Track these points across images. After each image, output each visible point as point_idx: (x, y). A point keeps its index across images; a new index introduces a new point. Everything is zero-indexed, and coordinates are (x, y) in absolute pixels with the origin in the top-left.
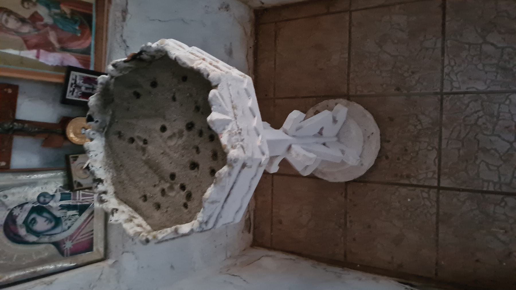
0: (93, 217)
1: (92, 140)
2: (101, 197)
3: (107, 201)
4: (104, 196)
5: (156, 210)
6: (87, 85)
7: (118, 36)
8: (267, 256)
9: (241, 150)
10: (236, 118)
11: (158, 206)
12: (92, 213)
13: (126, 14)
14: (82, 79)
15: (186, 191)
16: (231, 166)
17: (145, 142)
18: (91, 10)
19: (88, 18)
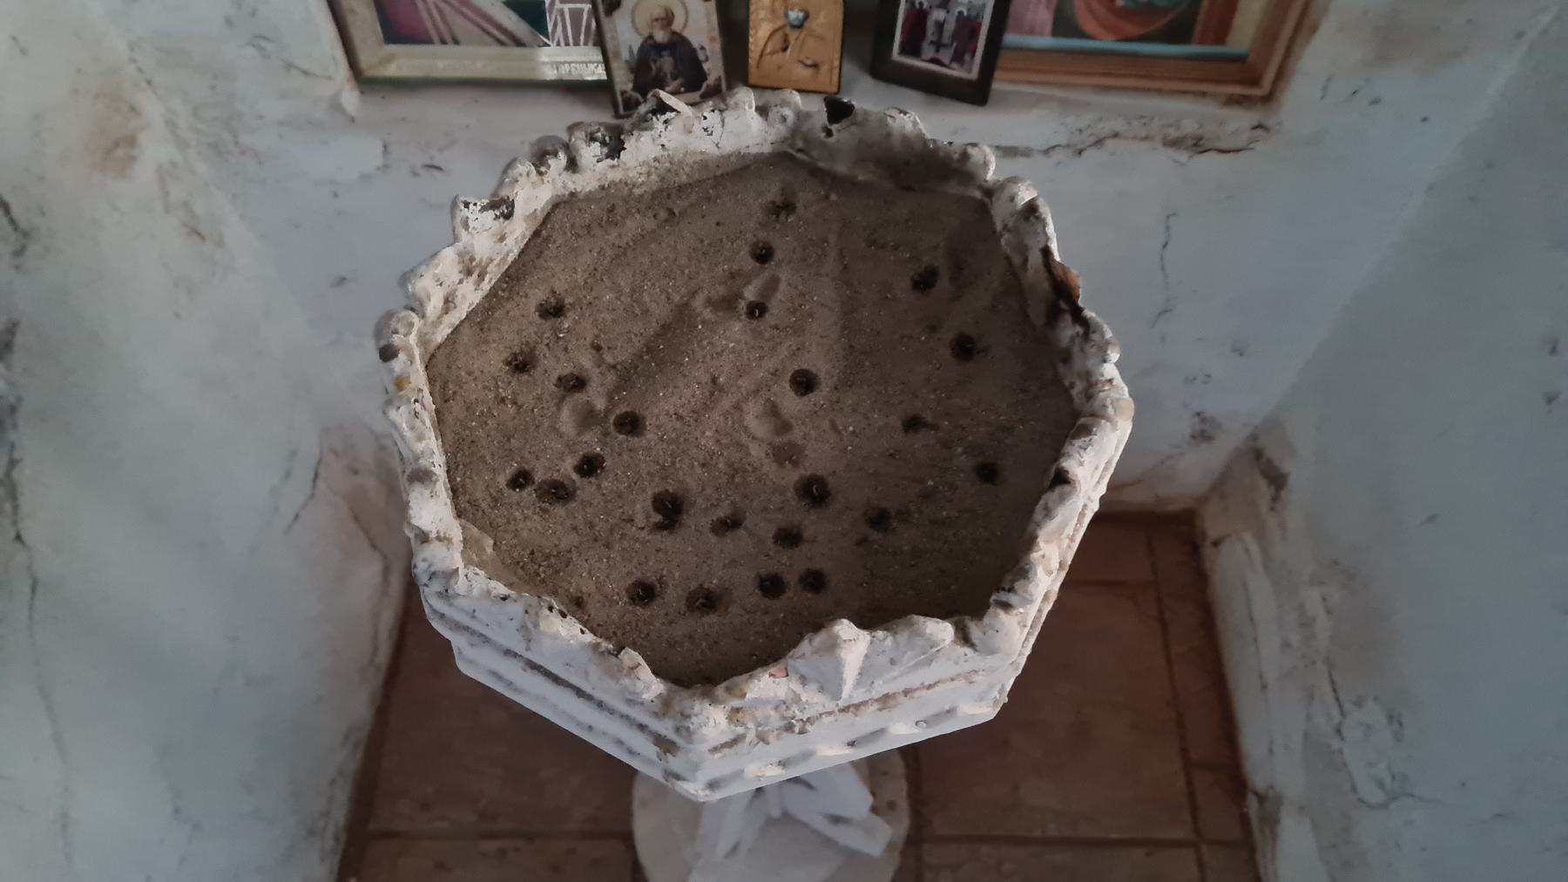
0: (501, 43)
1: (763, 111)
2: (555, 154)
3: (540, 174)
4: (558, 163)
5: (506, 355)
6: (950, 27)
7: (1118, 125)
8: (386, 570)
9: (727, 738)
10: (845, 710)
11: (521, 364)
12: (518, 43)
13: (1187, 148)
14: (974, 14)
15: (575, 476)
16: (665, 706)
17: (757, 310)
18: (1202, 42)
19: (1178, 32)
